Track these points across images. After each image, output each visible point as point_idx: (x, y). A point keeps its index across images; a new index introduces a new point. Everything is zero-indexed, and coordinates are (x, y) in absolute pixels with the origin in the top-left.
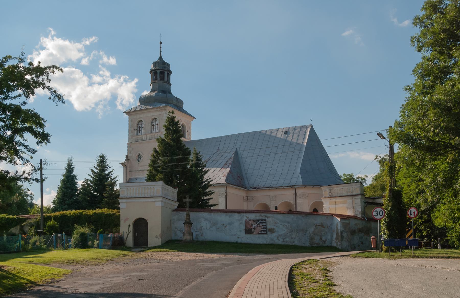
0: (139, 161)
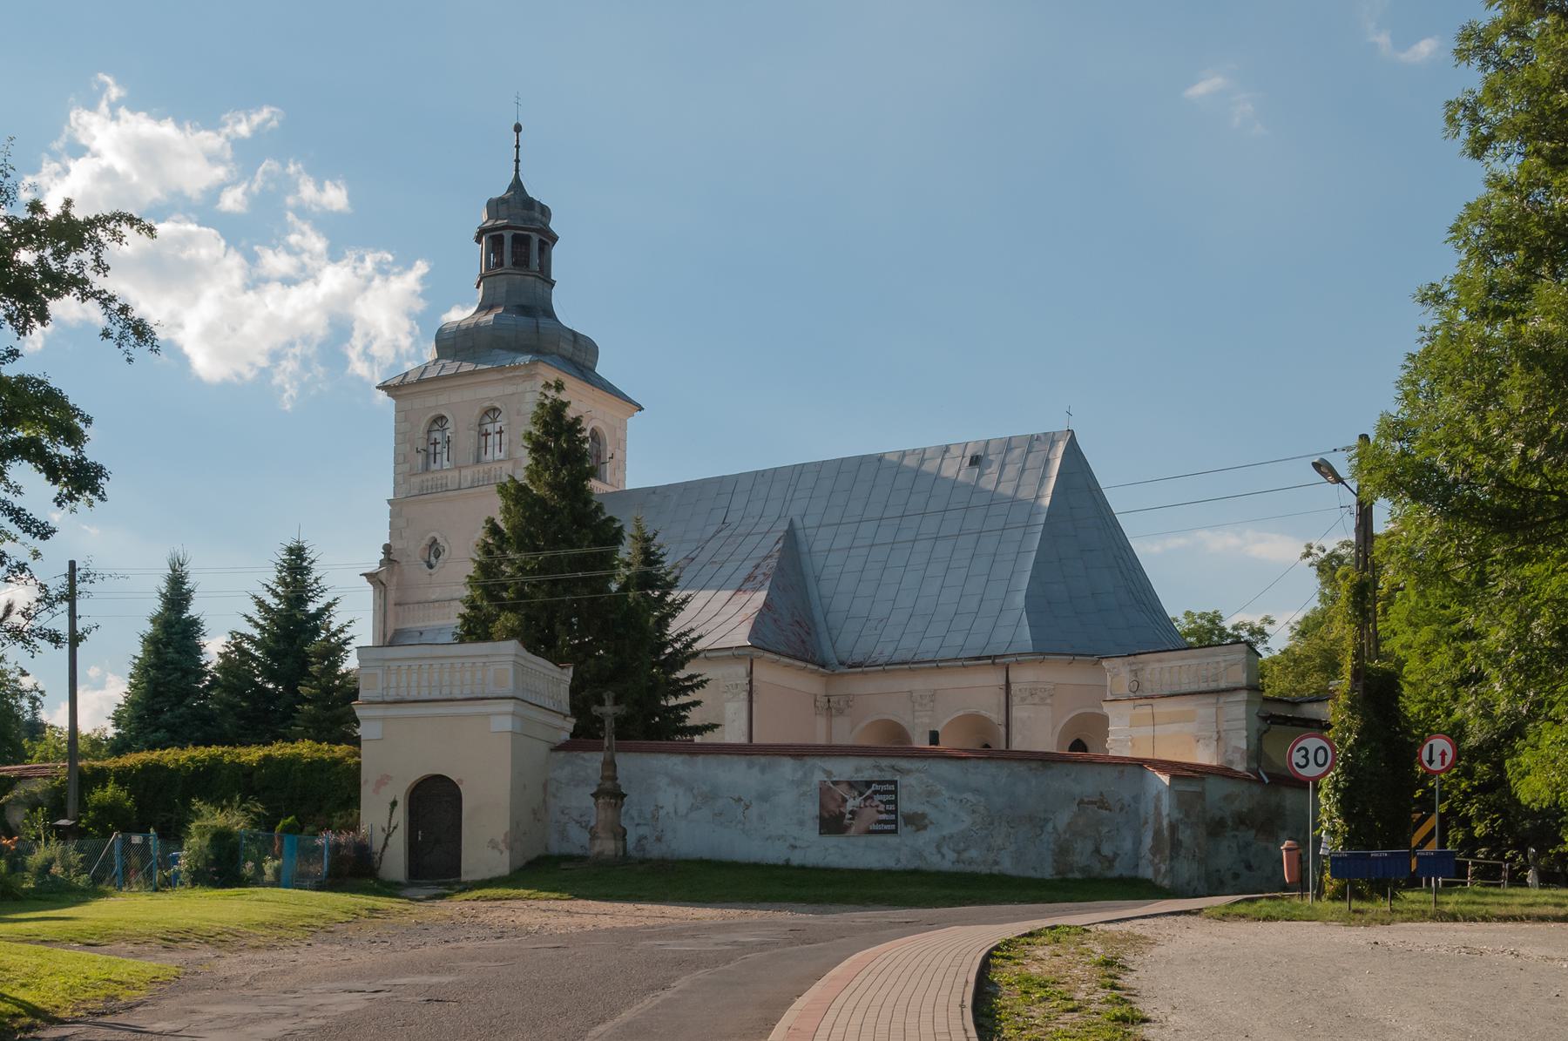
0: (431, 566)
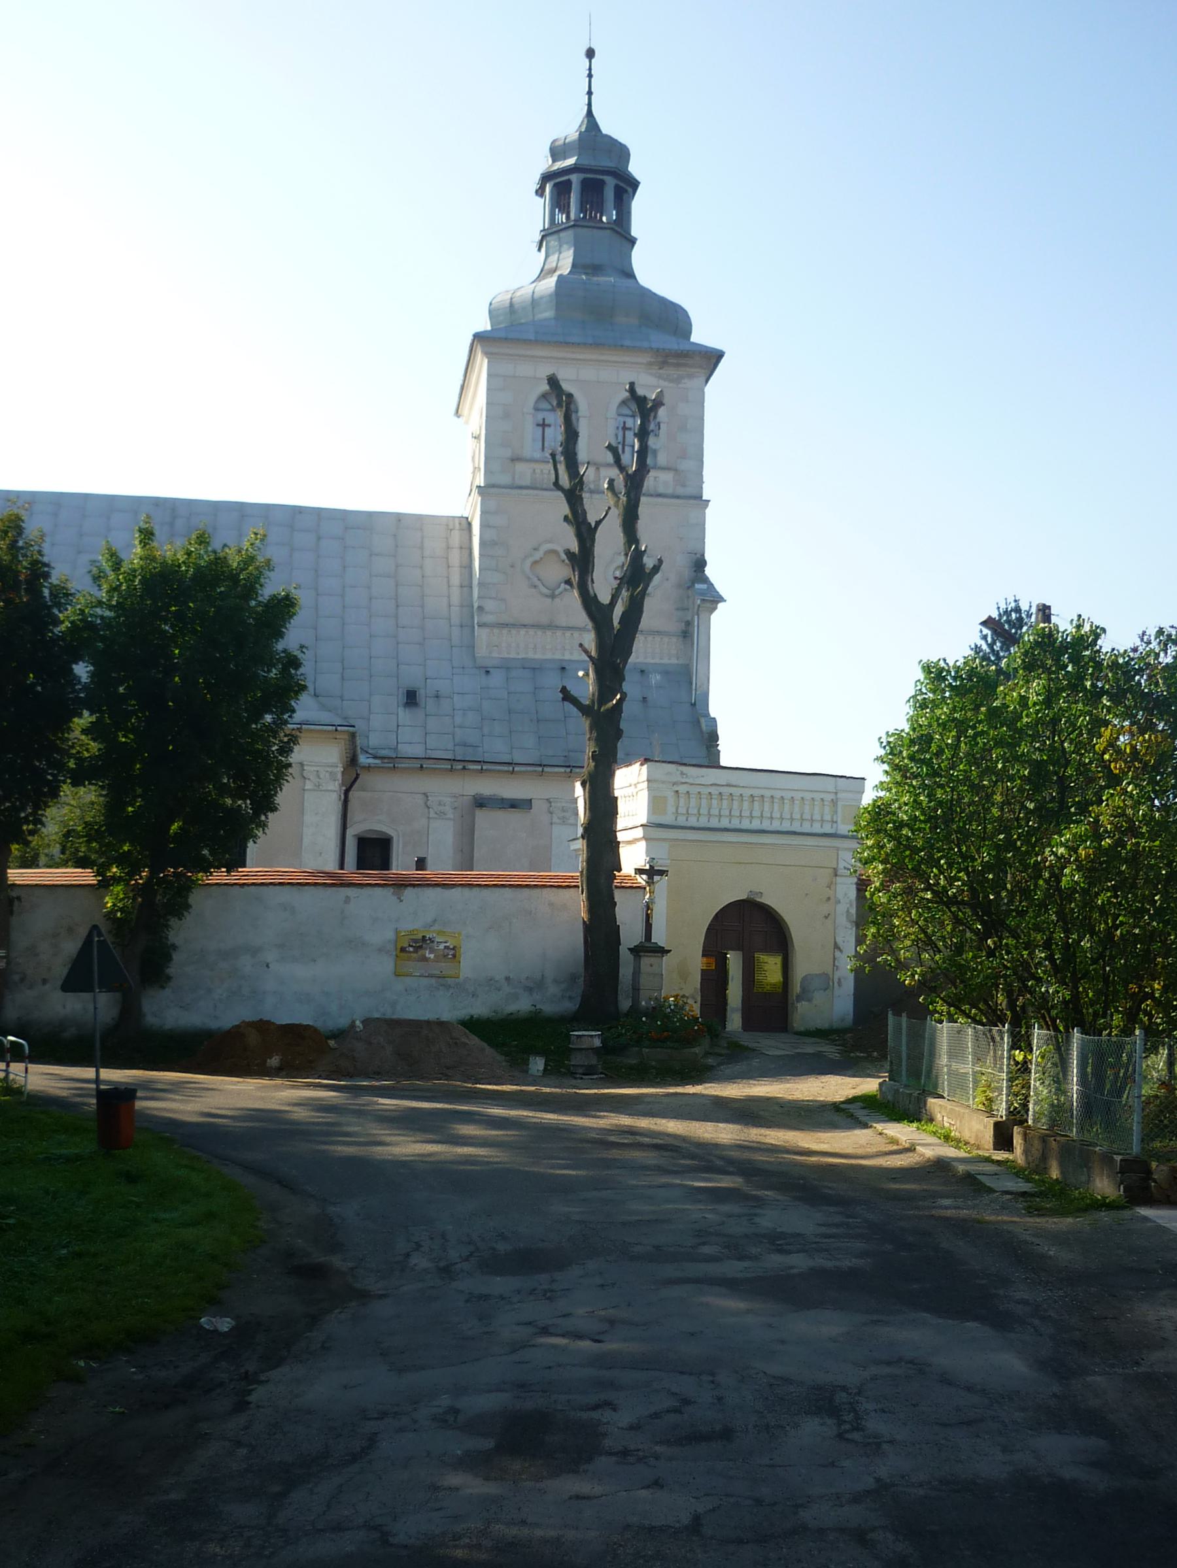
0: (545, 1492)
